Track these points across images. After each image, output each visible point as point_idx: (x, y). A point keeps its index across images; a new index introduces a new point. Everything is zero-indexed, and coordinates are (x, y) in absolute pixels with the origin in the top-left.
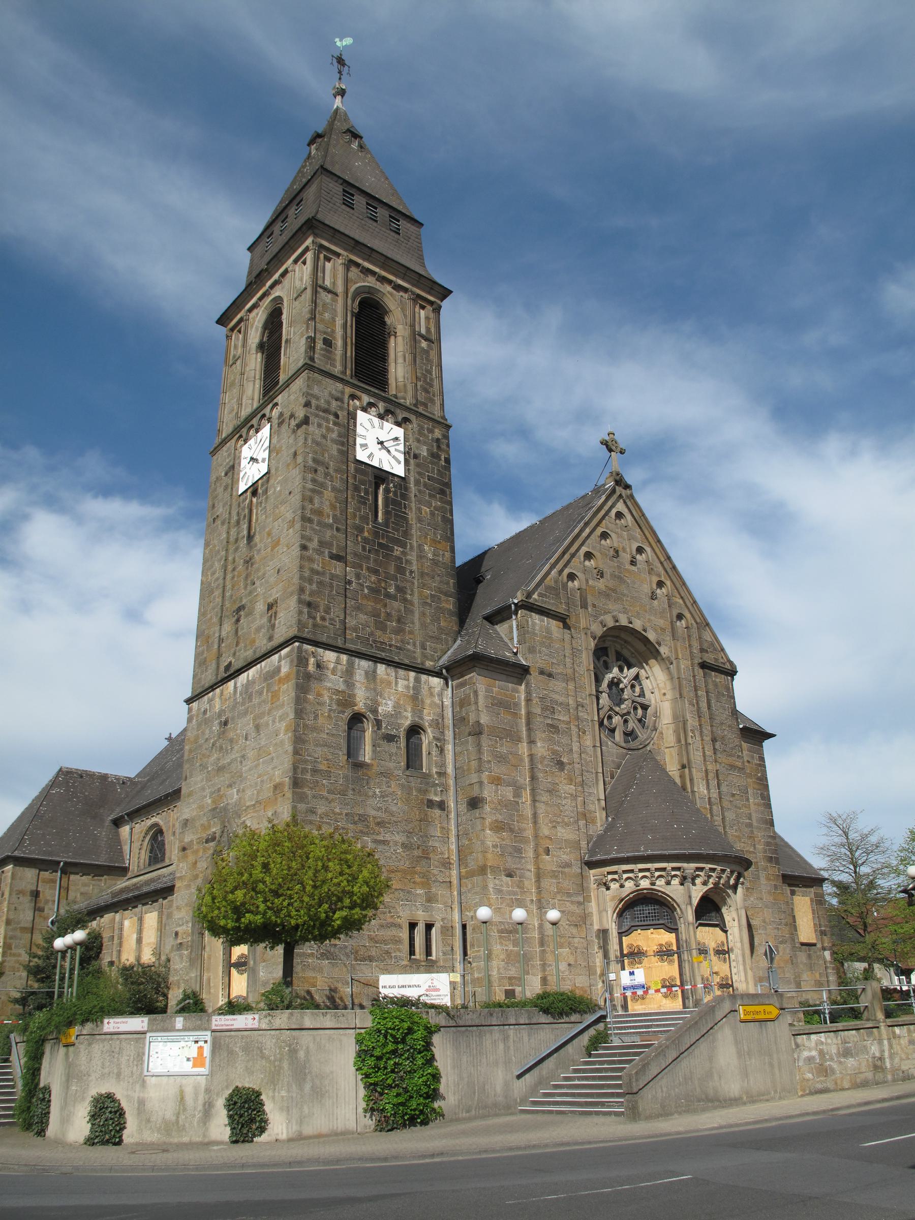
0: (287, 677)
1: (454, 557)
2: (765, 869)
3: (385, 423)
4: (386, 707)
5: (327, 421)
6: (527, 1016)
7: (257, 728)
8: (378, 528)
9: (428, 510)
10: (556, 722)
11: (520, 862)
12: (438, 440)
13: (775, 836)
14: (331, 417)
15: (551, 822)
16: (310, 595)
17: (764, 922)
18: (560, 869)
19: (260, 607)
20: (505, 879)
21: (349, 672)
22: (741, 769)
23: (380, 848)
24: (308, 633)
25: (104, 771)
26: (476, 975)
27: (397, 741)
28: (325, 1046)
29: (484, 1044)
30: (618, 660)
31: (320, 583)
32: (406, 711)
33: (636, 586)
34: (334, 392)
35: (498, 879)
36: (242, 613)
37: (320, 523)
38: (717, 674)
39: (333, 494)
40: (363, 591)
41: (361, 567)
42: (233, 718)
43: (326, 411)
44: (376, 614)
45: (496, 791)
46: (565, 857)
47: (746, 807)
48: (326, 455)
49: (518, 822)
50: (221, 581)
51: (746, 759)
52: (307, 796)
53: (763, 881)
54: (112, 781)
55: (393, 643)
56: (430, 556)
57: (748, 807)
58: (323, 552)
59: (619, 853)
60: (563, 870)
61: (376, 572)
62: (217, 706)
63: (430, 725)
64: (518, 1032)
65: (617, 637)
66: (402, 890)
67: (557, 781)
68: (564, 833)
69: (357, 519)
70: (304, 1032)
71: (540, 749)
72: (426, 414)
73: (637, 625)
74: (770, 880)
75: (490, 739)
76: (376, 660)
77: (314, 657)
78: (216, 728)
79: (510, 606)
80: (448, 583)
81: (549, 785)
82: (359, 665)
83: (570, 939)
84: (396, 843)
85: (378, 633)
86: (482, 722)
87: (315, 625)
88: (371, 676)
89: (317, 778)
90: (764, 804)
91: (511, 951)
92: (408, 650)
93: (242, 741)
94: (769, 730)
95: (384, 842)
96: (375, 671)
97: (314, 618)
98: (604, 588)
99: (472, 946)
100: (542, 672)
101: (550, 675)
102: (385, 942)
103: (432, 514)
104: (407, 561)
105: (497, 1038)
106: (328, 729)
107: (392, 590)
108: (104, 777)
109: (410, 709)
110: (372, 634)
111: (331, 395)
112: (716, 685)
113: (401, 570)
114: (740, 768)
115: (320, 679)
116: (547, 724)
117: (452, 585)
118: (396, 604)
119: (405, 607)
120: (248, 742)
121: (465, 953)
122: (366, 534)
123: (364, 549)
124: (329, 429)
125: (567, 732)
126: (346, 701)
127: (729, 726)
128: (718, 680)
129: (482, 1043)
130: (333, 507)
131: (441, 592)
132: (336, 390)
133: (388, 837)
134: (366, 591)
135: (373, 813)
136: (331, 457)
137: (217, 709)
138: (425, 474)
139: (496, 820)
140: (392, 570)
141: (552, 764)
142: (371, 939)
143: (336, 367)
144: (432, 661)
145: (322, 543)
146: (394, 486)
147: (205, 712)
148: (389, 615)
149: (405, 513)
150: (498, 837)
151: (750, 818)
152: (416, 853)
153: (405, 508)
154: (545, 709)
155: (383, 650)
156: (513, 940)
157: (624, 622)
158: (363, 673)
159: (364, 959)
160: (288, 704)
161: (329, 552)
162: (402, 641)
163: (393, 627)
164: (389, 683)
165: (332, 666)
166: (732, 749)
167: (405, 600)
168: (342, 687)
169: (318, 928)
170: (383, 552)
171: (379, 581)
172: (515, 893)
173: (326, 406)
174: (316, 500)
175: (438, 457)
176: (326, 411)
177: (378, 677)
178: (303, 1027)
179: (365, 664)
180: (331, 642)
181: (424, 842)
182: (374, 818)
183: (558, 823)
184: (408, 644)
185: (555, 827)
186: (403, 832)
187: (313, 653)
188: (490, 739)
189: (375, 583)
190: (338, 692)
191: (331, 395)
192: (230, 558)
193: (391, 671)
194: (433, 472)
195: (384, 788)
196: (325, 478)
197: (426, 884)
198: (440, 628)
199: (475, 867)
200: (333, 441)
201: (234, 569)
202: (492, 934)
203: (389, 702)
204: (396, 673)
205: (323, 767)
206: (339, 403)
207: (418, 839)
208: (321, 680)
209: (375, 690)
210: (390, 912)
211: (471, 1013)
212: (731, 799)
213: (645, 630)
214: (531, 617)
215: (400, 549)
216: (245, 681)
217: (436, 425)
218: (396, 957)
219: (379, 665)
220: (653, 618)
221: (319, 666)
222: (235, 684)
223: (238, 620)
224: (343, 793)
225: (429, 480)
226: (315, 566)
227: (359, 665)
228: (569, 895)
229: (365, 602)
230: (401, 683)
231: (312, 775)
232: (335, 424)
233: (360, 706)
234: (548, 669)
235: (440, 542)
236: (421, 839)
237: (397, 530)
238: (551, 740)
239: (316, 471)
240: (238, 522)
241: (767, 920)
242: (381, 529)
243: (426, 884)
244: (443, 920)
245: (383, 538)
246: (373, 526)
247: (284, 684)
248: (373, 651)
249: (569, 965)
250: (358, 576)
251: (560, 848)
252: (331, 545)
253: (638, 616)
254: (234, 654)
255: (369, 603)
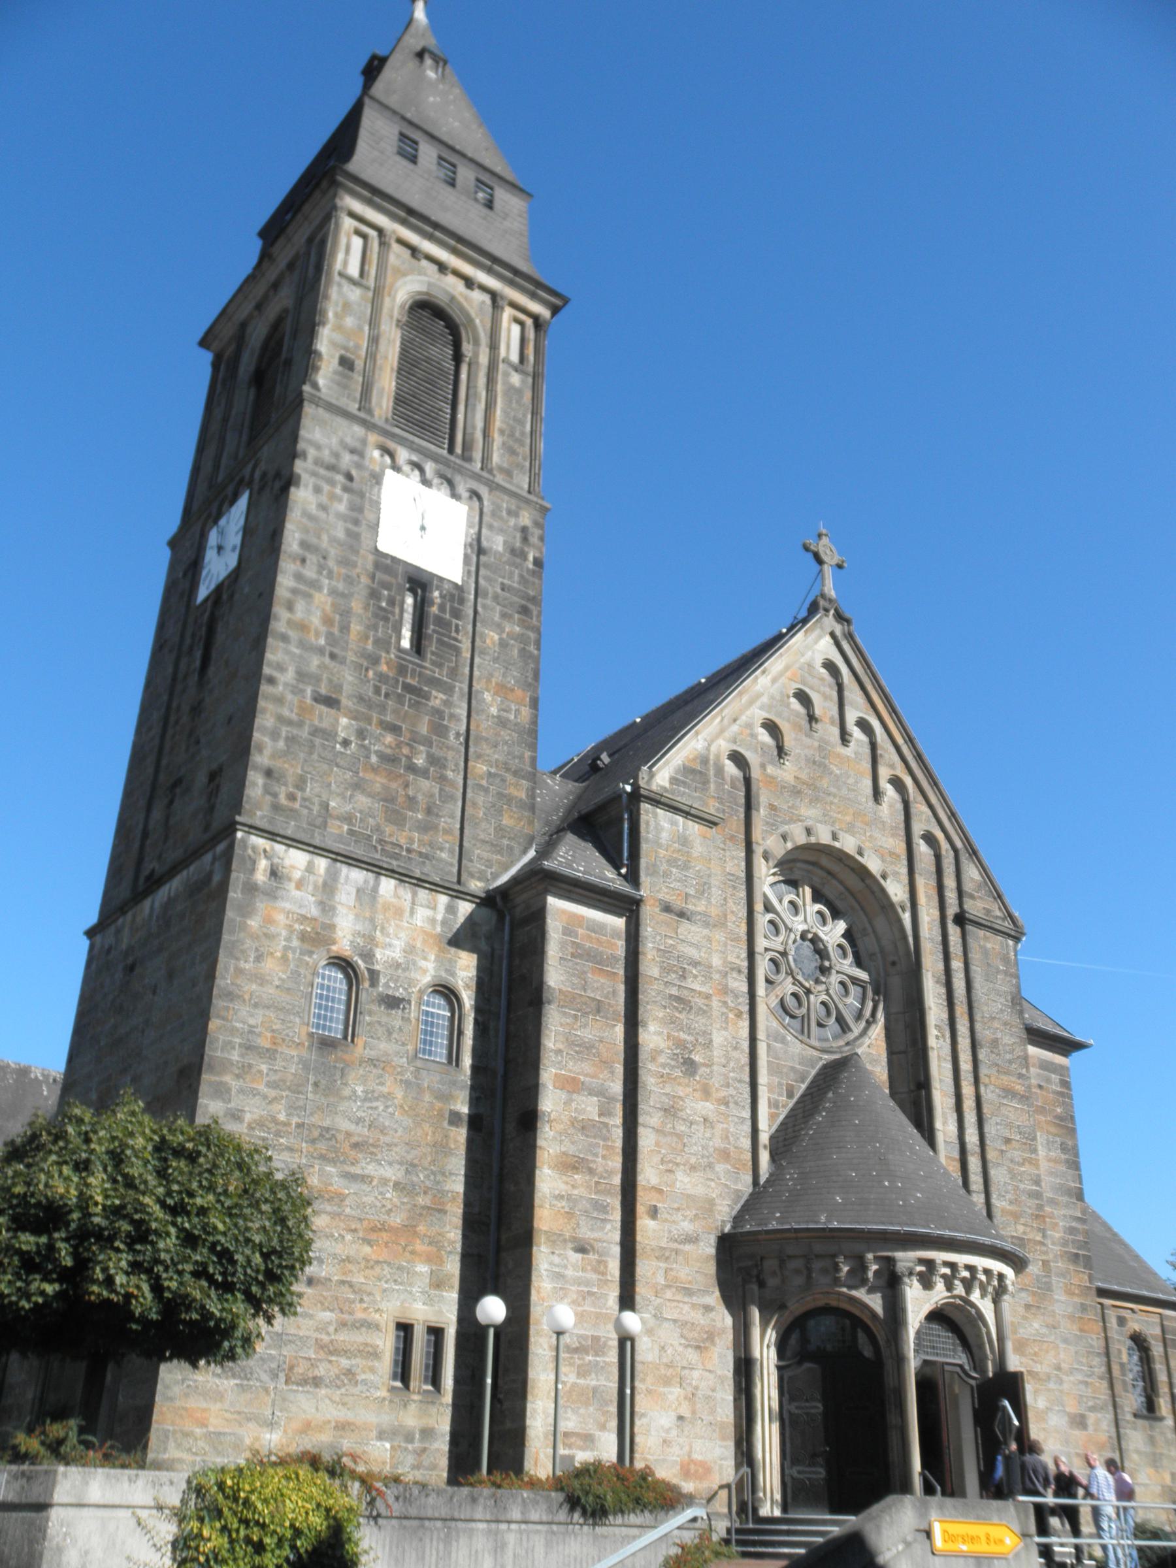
1: (536, 716)
2: (1062, 1275)
4: (388, 953)
5: (332, 483)
6: (545, 1507)
7: (170, 976)
8: (404, 659)
10: (686, 992)
11: (603, 1229)
12: (524, 530)
13: (1088, 1217)
14: (340, 478)
15: (662, 1162)
16: (273, 756)
17: (1058, 1368)
18: (675, 1246)
19: (201, 779)
21: (329, 887)
22: (1024, 1098)
23: (354, 1187)
24: (263, 817)
25: (24, 1063)
27: (404, 1008)
28: (123, 1543)
29: (454, 1555)
31: (291, 740)
32: (425, 959)
33: (851, 781)
34: (348, 440)
35: (559, 1255)
36: (178, 790)
37: (302, 644)
38: (988, 934)
39: (330, 600)
40: (368, 757)
41: (369, 720)
43: (332, 468)
44: (388, 799)
45: (567, 1103)
46: (687, 1226)
47: (1030, 1163)
48: (325, 537)
49: (604, 1157)
50: (157, 741)
51: (1034, 1082)
52: (228, 1090)
53: (1059, 1295)
54: (36, 1077)
55: (415, 846)
56: (494, 710)
57: (1035, 1163)
58: (302, 691)
59: (782, 1224)
60: (681, 1247)
61: (395, 729)
62: (125, 940)
64: (524, 1537)
65: (814, 864)
66: (389, 1264)
67: (681, 1094)
68: (685, 1182)
69: (370, 641)
70: (85, 1512)
71: (655, 1038)
72: (507, 486)
73: (848, 844)
74: (1073, 1294)
75: (565, 1013)
76: (377, 869)
77: (266, 857)
78: (119, 975)
79: (620, 796)
80: (521, 757)
81: (665, 1099)
82: (347, 877)
83: (686, 1372)
84: (384, 1181)
85: (388, 829)
87: (276, 807)
88: (368, 896)
89: (252, 1059)
90: (1067, 1161)
91: (574, 1385)
92: (441, 860)
94: (1079, 1038)
95: (364, 1179)
96: (375, 889)
97: (275, 795)
98: (792, 781)
100: (667, 908)
101: (682, 914)
102: (345, 1353)
103: (503, 644)
104: (452, 716)
105: (480, 1547)
106: (280, 979)
107: (420, 761)
108: (24, 1072)
109: (433, 957)
110: (378, 829)
111: (342, 442)
112: (985, 952)
113: (439, 730)
114: (1022, 1096)
115: (272, 895)
116: (671, 996)
118: (425, 784)
119: (441, 790)
123: (377, 691)
124: (333, 497)
125: (705, 1012)
127: (1005, 1024)
128: (989, 946)
129: (450, 1553)
130: (328, 621)
131: (508, 770)
132: (352, 437)
133: (371, 1169)
134: (374, 759)
135: (345, 1125)
136: (333, 540)
137: (124, 946)
138: (496, 581)
139: (564, 1153)
140: (424, 729)
141: (673, 1063)
142: (322, 1347)
144: (479, 879)
145: (301, 675)
146: (442, 596)
148: (412, 801)
149: (456, 640)
150: (567, 1183)
151: (1037, 1182)
152: (421, 1200)
153: (457, 631)
154: (667, 970)
155: (396, 857)
156: (579, 1367)
157: (825, 838)
158: (354, 891)
159: (304, 1382)
161: (314, 691)
162: (431, 844)
163: (418, 821)
164: (399, 912)
165: (297, 875)
166: (1010, 1062)
167: (443, 779)
168: (314, 911)
170: (410, 700)
171: (399, 745)
172: (588, 1283)
173: (333, 461)
174: (300, 606)
175: (524, 556)
176: (332, 468)
177: (380, 900)
178: (85, 1501)
179: (358, 876)
180: (301, 836)
181: (438, 1183)
182: (348, 1134)
183: (677, 1164)
184: (441, 849)
185: (670, 1171)
186: (401, 1164)
187: (265, 851)
188: (565, 1013)
189: (391, 747)
190: (303, 919)
191: (342, 442)
192: (174, 705)
193: (406, 893)
194: (511, 578)
196: (320, 573)
198: (499, 829)
200: (339, 516)
201: (177, 723)
202: (540, 1351)
203: (395, 942)
204: (414, 894)
205: (264, 1042)
206: (356, 458)
207: (427, 1177)
208: (275, 898)
209: (372, 920)
210: (362, 1301)
211: (434, 1495)
212: (1004, 1148)
213: (884, 877)
214: (655, 815)
215: (441, 696)
217: (523, 505)
218: (364, 1382)
219: (383, 879)
221: (274, 873)
222: (153, 902)
223: (171, 802)
224: (297, 1089)
225: (503, 589)
226: (286, 713)
227: (347, 877)
228: (688, 1292)
229: (369, 776)
230: (422, 914)
231: (242, 1055)
232: (346, 489)
234: (678, 903)
236: (432, 1177)
237: (440, 666)
238: (673, 1021)
239: (303, 561)
240: (191, 648)
241: (1064, 1366)
242: (410, 662)
245: (413, 677)
246: (397, 657)
248: (359, 852)
249: (681, 1418)
250: (361, 734)
251: (678, 1209)
252: (318, 679)
253: (850, 829)
254: (160, 857)
255: (378, 779)
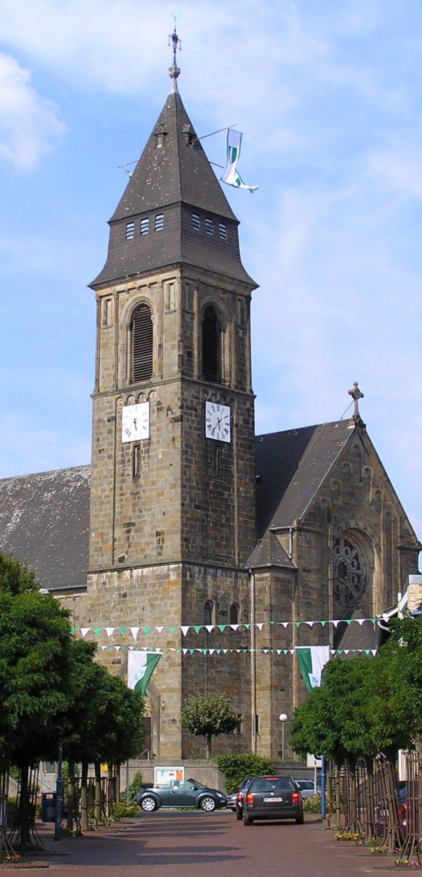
0: (175, 583)
3: (220, 406)
9: (242, 462)
20: (280, 692)
26: (263, 743)
30: (345, 545)
42: (131, 595)
63: (242, 603)
77: (189, 571)
86: (272, 604)
93: (139, 610)
99: (261, 727)
100: (304, 571)
101: (309, 571)
117: (254, 511)
120: (145, 612)
121: (257, 731)
122: (211, 487)
126: (204, 595)
134: (211, 524)
143: (193, 372)
147: (105, 583)
148: (222, 537)
160: (177, 598)
169: (222, 721)
195: (220, 642)
197: (239, 694)
199: (265, 685)
216: (140, 575)
220: (370, 518)
233: (210, 597)
235: (248, 484)
243: (239, 694)
244: (246, 712)
247: (173, 586)
